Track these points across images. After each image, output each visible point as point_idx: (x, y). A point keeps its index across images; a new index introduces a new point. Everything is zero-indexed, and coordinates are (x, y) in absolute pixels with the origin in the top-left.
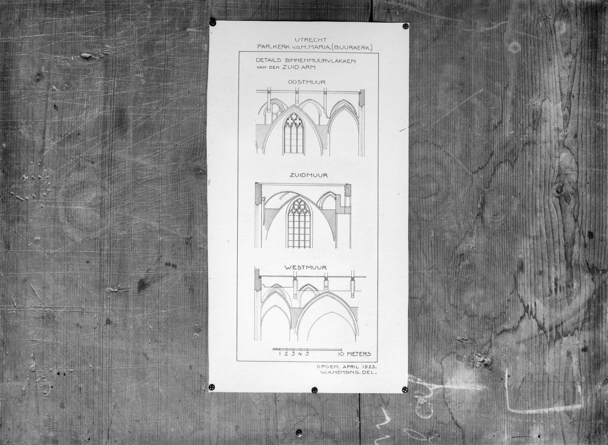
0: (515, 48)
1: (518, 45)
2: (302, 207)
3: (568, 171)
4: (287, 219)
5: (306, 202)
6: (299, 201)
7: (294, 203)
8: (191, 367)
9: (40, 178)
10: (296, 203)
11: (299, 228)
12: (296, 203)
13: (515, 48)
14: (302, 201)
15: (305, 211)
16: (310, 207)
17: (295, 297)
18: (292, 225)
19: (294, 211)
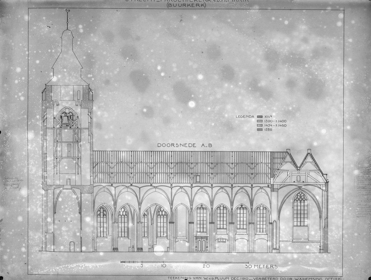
0: (69, 203)
1: (69, 204)
2: (303, 197)
3: (12, 267)
4: (308, 212)
5: (305, 193)
6: (301, 193)
7: (297, 195)
8: (244, 139)
9: (232, 187)
10: (299, 195)
11: (240, 217)
12: (299, 195)
13: (69, 203)
14: (302, 193)
15: (304, 199)
16: (295, 196)
17: (210, 146)
18: (243, 212)
19: (297, 199)
